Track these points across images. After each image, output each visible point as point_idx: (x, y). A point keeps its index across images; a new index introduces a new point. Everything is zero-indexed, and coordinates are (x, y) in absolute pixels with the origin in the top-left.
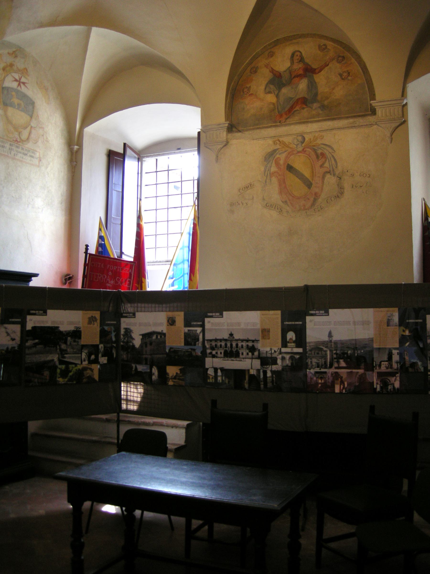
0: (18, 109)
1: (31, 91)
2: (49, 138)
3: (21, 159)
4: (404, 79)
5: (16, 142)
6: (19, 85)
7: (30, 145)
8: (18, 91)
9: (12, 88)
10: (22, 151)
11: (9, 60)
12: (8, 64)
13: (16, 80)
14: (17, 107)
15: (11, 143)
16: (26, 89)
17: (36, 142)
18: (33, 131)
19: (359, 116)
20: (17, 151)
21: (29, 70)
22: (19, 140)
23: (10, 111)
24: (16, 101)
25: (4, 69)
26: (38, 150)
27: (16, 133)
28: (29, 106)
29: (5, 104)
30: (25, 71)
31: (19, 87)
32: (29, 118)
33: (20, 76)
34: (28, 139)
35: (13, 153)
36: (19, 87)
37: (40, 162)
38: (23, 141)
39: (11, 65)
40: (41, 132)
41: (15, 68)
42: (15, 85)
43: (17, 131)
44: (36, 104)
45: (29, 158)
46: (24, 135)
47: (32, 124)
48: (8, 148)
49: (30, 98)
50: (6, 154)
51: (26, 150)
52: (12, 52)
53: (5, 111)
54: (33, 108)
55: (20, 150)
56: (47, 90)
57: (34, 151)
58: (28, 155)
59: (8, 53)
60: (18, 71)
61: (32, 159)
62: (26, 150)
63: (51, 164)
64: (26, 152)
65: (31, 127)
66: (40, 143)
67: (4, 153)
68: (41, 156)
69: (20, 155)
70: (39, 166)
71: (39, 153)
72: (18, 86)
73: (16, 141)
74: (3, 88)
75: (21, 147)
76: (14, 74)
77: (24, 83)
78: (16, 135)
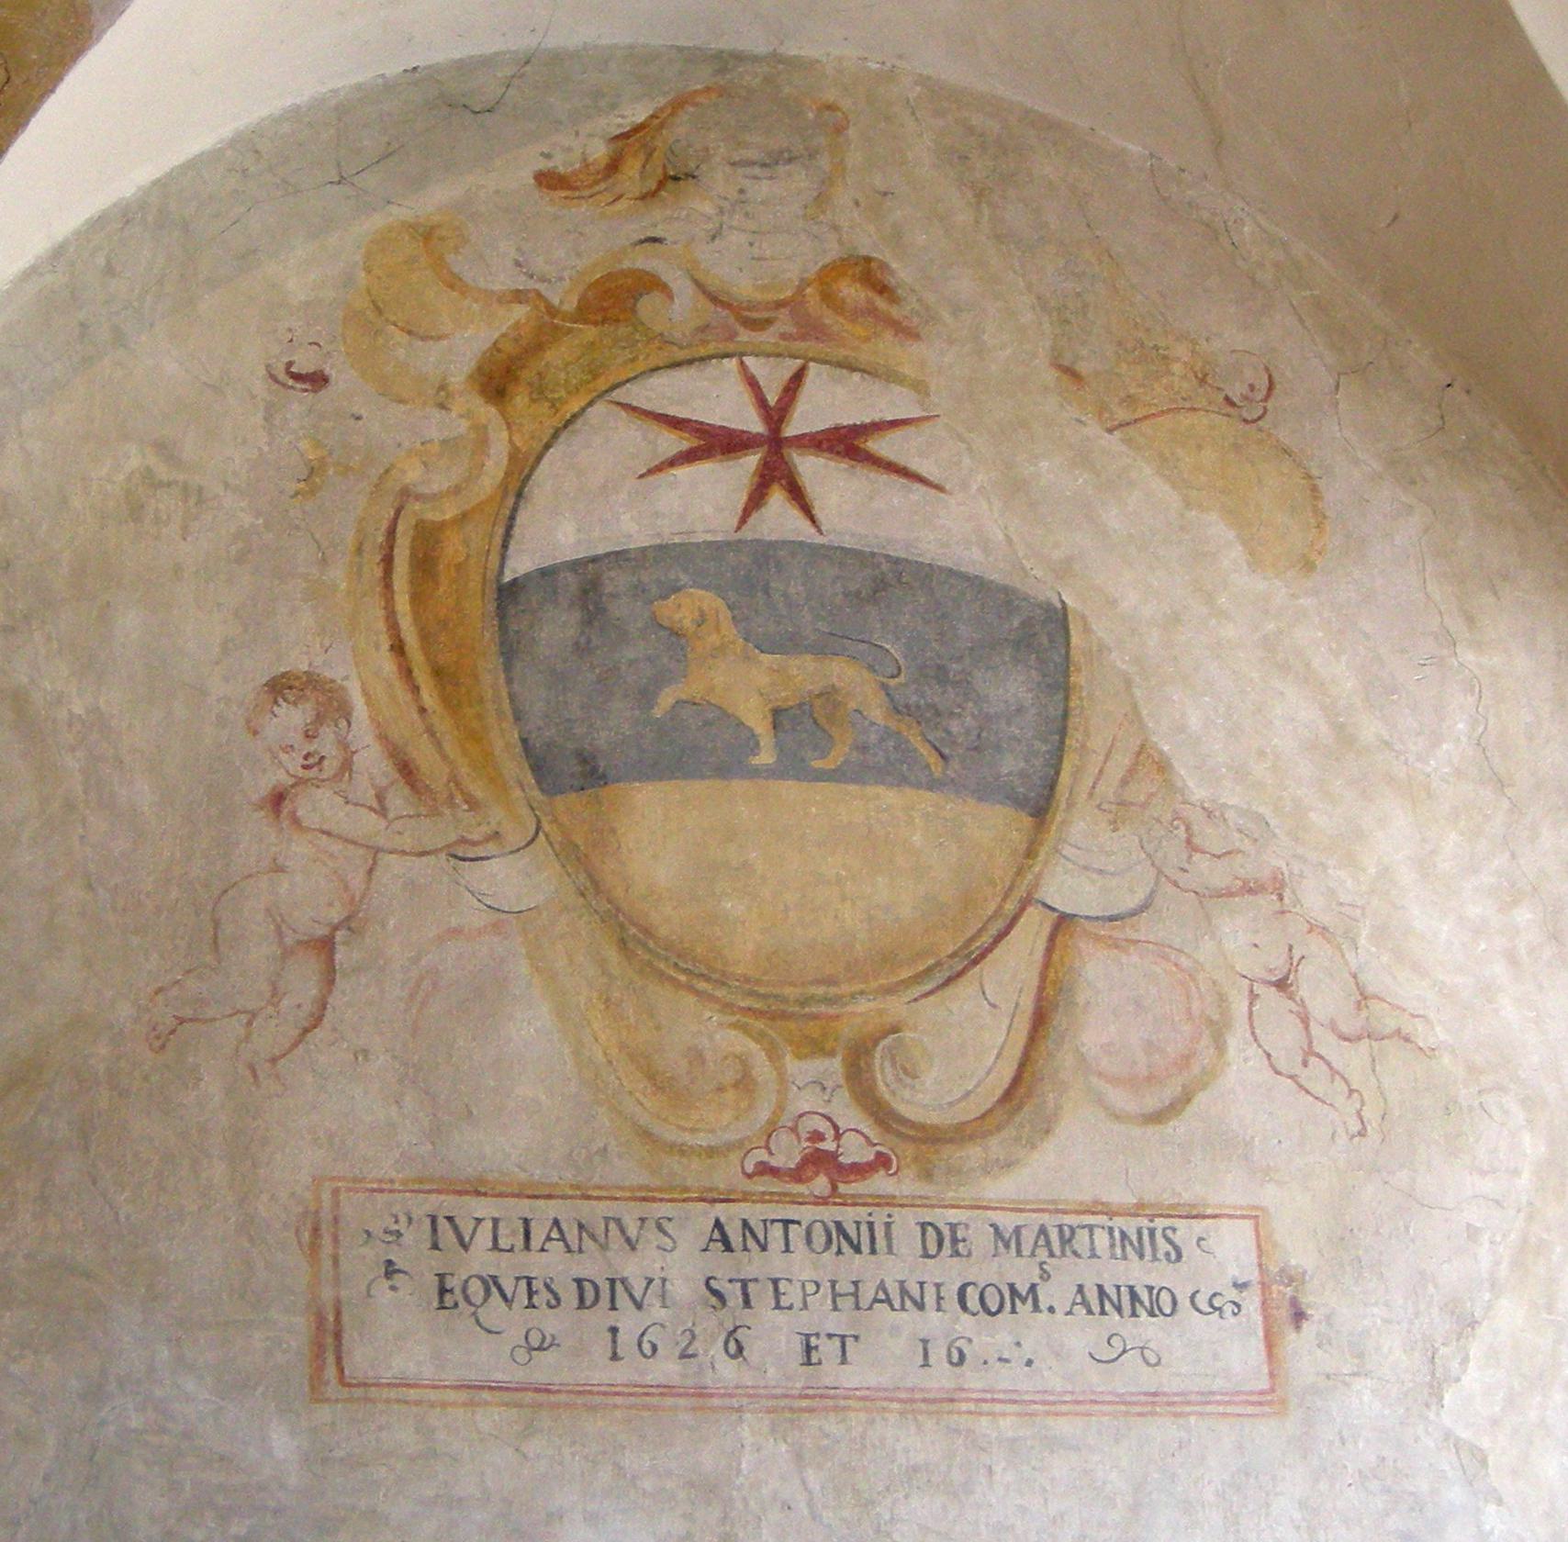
0: (792, 767)
1: (966, 499)
2: (1408, 990)
3: (940, 1377)
4: (751, 499)
5: (821, 1184)
6: (775, 475)
7: (1075, 1159)
8: (767, 554)
9: (669, 560)
10: (949, 1272)
11: (577, 246)
12: (564, 297)
13: (717, 443)
14: (766, 757)
15: (731, 1214)
16: (893, 493)
17: (1169, 1096)
18: (1096, 970)
19: (505, 546)
20: (849, 1296)
21: (902, 273)
22: (854, 1151)
23: (661, 835)
24: (745, 686)
25: (496, 381)
26: (1230, 1189)
27: (801, 1069)
28: (988, 691)
29: (573, 770)
30: (852, 292)
31: (777, 498)
32: (995, 826)
33: (772, 376)
34: (1018, 1091)
35: (774, 1334)
36: (777, 498)
37: (1299, 1344)
38: (931, 1137)
39: (615, 298)
40: (1239, 940)
41: (679, 310)
42: (708, 498)
43: (816, 1047)
44: (1096, 630)
45: (1081, 1335)
46: (958, 1046)
47: (1066, 887)
48: (684, 1288)
49: (978, 585)
50: (666, 1369)
51: (1006, 1240)
52: (599, 151)
53: (585, 864)
54: (1058, 681)
55: (901, 1264)
56: (1249, 405)
57: (1153, 1227)
58: (1056, 1293)
59: (548, 180)
60: (733, 321)
61: (1148, 1328)
62: (1006, 1240)
63: (1509, 1315)
64: (1020, 1272)
65: (1063, 922)
66: (1244, 1085)
67: (620, 1374)
68: (1299, 1253)
69: (895, 1332)
70: (1271, 1397)
71: (1256, 1217)
72: (756, 499)
73: (818, 1161)
74: (508, 594)
75: (905, 1222)
76: (663, 392)
77: (845, 443)
78: (812, 1093)
